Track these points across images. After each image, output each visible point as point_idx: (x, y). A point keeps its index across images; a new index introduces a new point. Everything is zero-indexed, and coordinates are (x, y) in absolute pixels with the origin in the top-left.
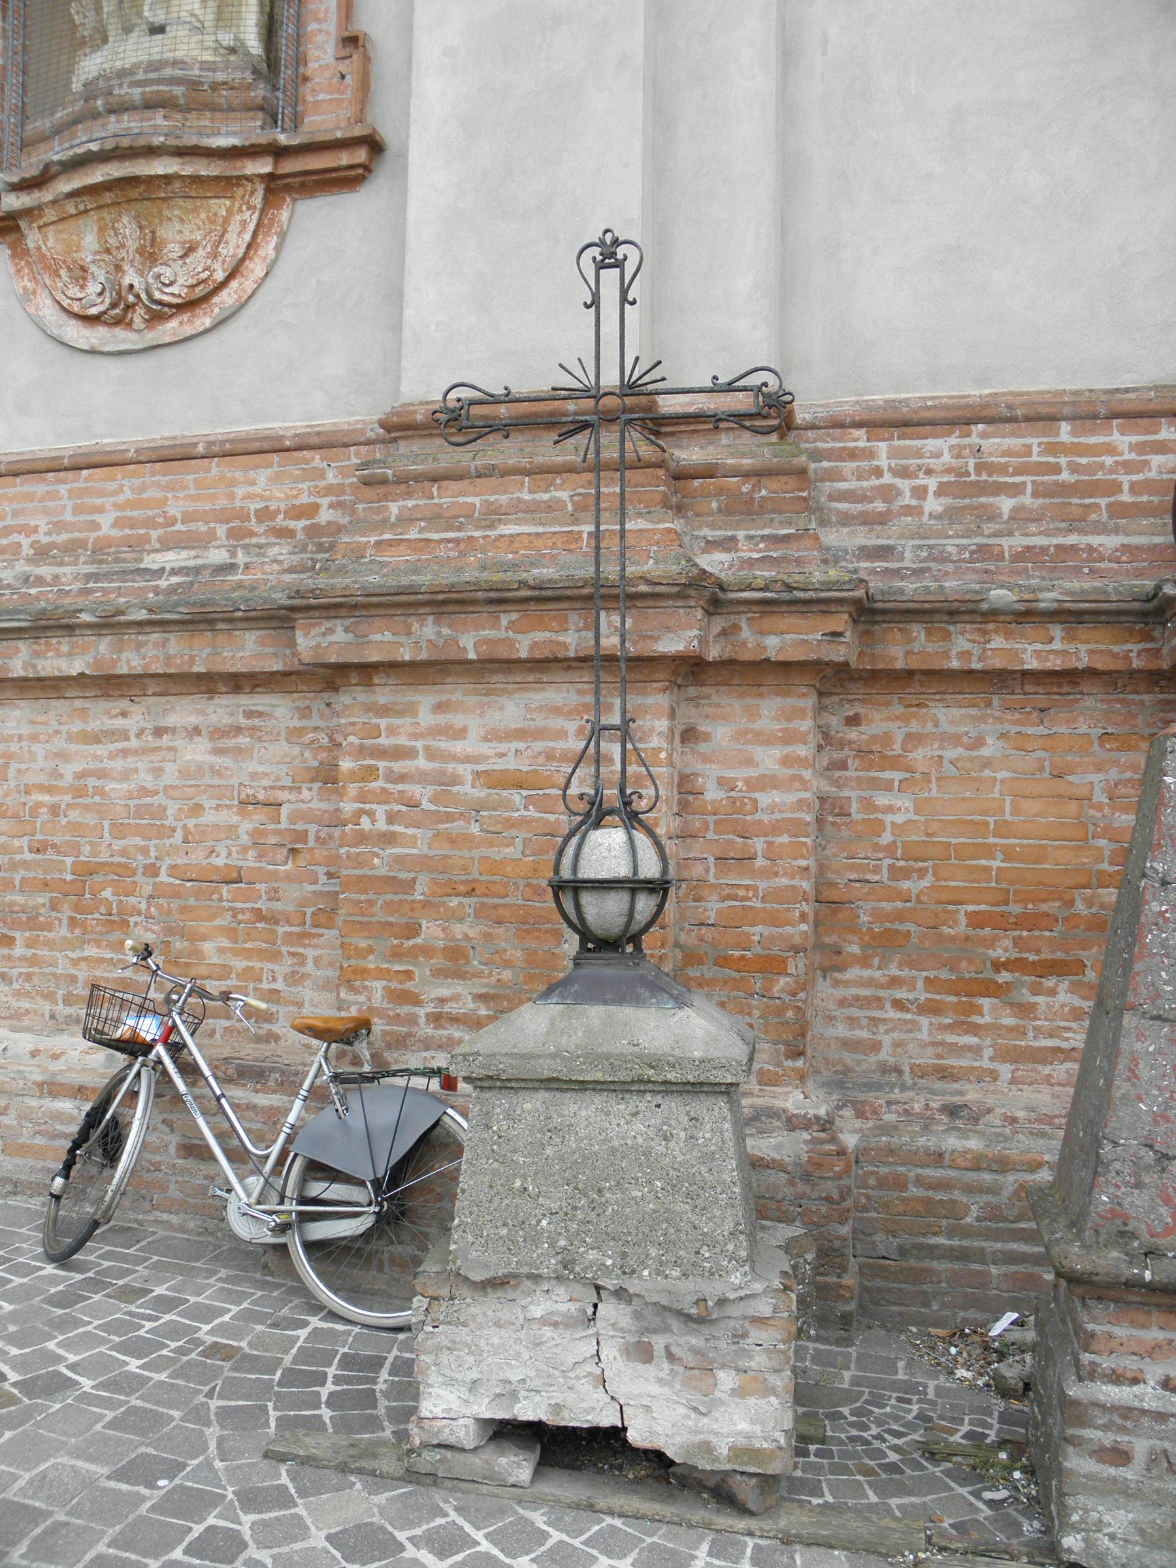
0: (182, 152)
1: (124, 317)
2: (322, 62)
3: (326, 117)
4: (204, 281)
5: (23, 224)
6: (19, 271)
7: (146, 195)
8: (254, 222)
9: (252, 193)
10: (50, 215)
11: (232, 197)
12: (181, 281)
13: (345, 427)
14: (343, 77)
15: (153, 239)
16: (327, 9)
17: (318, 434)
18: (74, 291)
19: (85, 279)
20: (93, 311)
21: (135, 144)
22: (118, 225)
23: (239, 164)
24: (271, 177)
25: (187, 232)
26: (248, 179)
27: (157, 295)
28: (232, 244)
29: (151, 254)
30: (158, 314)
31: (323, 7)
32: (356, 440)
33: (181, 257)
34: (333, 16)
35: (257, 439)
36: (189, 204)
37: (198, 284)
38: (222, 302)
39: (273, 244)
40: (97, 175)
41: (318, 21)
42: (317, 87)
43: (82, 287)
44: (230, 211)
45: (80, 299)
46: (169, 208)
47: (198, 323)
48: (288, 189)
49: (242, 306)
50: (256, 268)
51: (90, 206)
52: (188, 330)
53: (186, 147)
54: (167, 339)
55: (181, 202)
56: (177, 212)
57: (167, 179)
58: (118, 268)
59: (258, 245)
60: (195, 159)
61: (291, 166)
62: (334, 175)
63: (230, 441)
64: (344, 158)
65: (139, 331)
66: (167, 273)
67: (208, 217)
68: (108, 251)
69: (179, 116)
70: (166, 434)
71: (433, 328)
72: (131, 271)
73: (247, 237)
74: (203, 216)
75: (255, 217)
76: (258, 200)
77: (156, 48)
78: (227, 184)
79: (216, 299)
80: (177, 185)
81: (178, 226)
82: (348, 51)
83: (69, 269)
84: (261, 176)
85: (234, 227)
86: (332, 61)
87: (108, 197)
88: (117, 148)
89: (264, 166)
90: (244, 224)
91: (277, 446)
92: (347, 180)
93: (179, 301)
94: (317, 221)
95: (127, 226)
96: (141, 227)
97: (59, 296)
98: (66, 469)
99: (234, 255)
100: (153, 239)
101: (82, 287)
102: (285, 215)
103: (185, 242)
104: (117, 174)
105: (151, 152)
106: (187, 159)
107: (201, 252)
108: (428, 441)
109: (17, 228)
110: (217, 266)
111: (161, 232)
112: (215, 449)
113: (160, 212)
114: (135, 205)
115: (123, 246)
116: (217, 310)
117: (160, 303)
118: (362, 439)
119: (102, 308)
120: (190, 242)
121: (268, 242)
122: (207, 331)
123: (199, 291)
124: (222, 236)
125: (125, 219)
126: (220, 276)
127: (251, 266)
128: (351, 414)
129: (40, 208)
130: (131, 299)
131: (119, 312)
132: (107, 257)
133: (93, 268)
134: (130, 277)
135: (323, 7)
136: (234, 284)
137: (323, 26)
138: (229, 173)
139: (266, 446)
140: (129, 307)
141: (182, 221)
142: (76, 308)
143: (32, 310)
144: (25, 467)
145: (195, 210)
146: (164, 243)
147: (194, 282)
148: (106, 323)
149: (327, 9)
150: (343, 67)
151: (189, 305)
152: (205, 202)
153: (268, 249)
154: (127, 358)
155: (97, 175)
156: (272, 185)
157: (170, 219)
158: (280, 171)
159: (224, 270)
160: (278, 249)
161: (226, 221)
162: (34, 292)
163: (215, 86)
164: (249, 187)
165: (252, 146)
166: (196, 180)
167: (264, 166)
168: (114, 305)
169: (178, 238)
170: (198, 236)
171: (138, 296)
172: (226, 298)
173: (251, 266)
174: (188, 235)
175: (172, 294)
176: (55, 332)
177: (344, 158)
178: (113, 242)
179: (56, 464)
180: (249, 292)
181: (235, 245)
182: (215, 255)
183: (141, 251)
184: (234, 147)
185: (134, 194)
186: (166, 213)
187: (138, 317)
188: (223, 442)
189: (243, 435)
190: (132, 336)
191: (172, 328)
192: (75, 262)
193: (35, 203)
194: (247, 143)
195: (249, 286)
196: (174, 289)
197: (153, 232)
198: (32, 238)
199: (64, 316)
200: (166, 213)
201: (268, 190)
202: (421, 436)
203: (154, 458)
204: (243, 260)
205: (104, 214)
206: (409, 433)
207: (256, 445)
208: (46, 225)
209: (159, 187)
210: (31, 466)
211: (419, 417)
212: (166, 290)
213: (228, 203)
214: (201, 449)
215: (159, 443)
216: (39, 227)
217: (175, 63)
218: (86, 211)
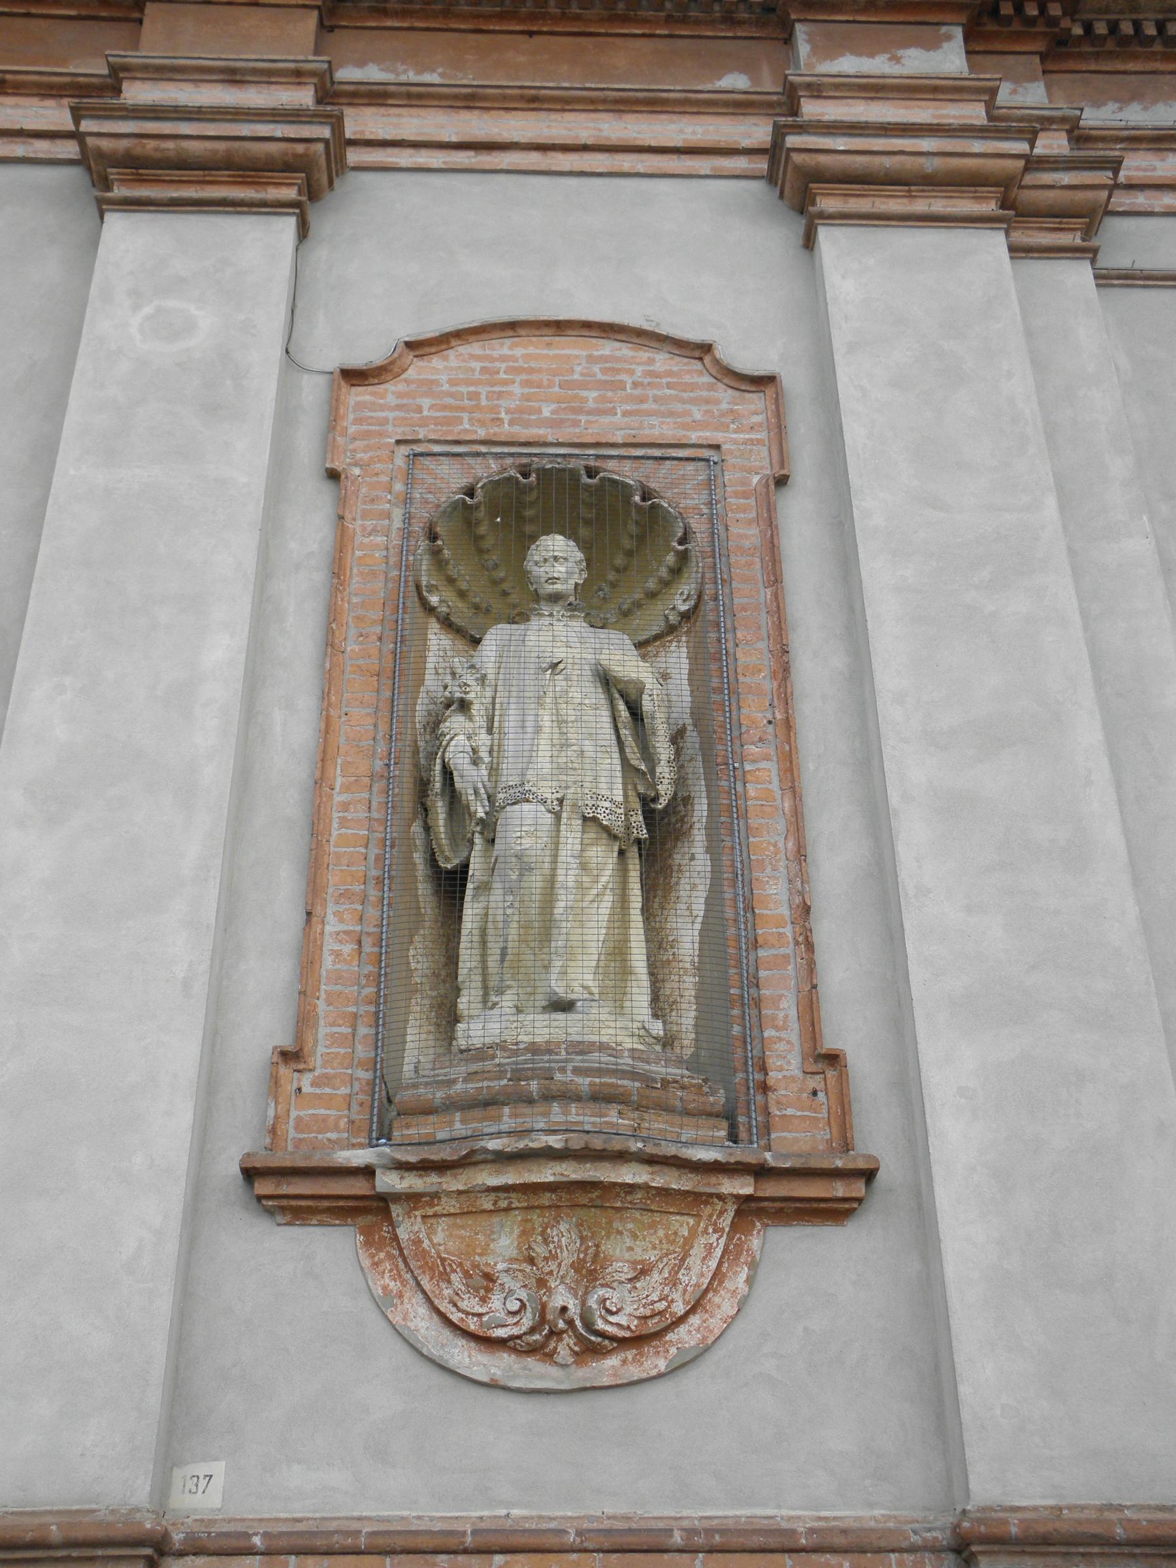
0: (651, 1161)
1: (544, 1345)
2: (788, 1074)
3: (797, 1136)
4: (660, 1313)
5: (396, 1210)
6: (376, 1264)
7: (599, 1202)
8: (722, 1246)
9: (721, 1213)
10: (449, 1205)
11: (698, 1216)
12: (629, 1309)
13: (872, 1524)
14: (815, 1093)
15: (596, 1255)
16: (786, 1016)
17: (844, 1532)
18: (471, 1303)
19: (488, 1290)
20: (501, 1333)
21: (608, 1147)
22: (552, 1232)
23: (713, 1180)
24: (749, 1198)
25: (639, 1250)
26: (721, 1197)
27: (600, 1325)
28: (695, 1270)
29: (589, 1272)
30: (593, 1346)
31: (781, 1015)
32: (896, 1545)
33: (630, 1280)
34: (794, 1025)
35: (755, 1532)
36: (646, 1218)
37: (652, 1317)
38: (680, 1341)
39: (743, 1276)
40: (547, 1174)
41: (777, 1028)
42: (784, 1100)
43: (484, 1300)
44: (693, 1233)
45: (480, 1315)
46: (621, 1219)
47: (648, 1364)
48: (761, 1213)
49: (707, 1349)
50: (723, 1304)
51: (516, 1204)
52: (635, 1372)
53: (665, 1157)
54: (606, 1381)
55: (637, 1215)
56: (630, 1226)
57: (631, 1188)
58: (542, 1283)
59: (724, 1275)
60: (666, 1169)
61: (772, 1189)
62: (823, 1205)
63: (723, 1532)
64: (839, 1189)
65: (564, 1366)
66: (614, 1297)
67: (666, 1236)
68: (531, 1261)
69: (636, 1114)
70: (609, 1511)
71: (998, 1412)
72: (561, 1288)
73: (713, 1264)
74: (661, 1233)
75: (723, 1241)
76: (726, 1222)
77: (543, 1028)
78: (695, 1200)
79: (670, 1337)
80: (639, 1195)
81: (629, 1242)
82: (819, 1067)
83: (467, 1274)
84: (737, 1197)
85: (697, 1251)
86: (798, 1073)
87: (546, 1199)
88: (586, 1148)
89: (744, 1187)
90: (709, 1248)
91: (788, 1543)
92: (835, 1212)
93: (627, 1334)
94: (785, 1247)
95: (565, 1235)
96: (582, 1238)
97: (445, 1307)
98: (466, 1551)
99: (697, 1285)
100: (596, 1255)
101: (484, 1300)
102: (755, 1243)
103: (634, 1263)
104: (574, 1177)
105: (622, 1157)
106: (657, 1168)
107: (656, 1276)
108: (1017, 1559)
109: (386, 1213)
110: (676, 1295)
111: (607, 1247)
112: (699, 1540)
113: (610, 1223)
114: (581, 1212)
115: (554, 1257)
116: (673, 1351)
117: (602, 1334)
118: (904, 1544)
119: (516, 1331)
120: (642, 1262)
121: (736, 1273)
122: (660, 1376)
123: (653, 1325)
124: (683, 1260)
125: (563, 1227)
126: (679, 1308)
127: (717, 1300)
128: (871, 1505)
129: (435, 1196)
130: (561, 1325)
131: (537, 1344)
132: (528, 1269)
133: (505, 1279)
134: (561, 1297)
135: (781, 1015)
136: (695, 1320)
137: (783, 1034)
138: (701, 1189)
139: (773, 1542)
140: (554, 1334)
141: (635, 1237)
142: (472, 1325)
143: (397, 1319)
144: (400, 1542)
145: (653, 1226)
146: (608, 1260)
147: (648, 1313)
148: (515, 1350)
149: (786, 1016)
150: (814, 1082)
151: (637, 1341)
152: (665, 1217)
153: (738, 1280)
154: (543, 1399)
155: (547, 1174)
156: (744, 1207)
157: (620, 1233)
158: (760, 1194)
159: (686, 1303)
160: (750, 1281)
161: (688, 1243)
162: (400, 1296)
163: (665, 1083)
164: (719, 1205)
165: (737, 1163)
166: (664, 1192)
167: (744, 1187)
168: (532, 1330)
169: (627, 1256)
170: (652, 1256)
171: (570, 1323)
172: (686, 1336)
173: (717, 1300)
174: (639, 1254)
175: (618, 1325)
176: (435, 1352)
177: (839, 1189)
178: (540, 1250)
179: (452, 1543)
180: (717, 1332)
181: (697, 1271)
182: (673, 1282)
183: (577, 1266)
184: (716, 1162)
185: (583, 1199)
186: (617, 1225)
187: (564, 1348)
188: (709, 1532)
189: (731, 1524)
190: (554, 1371)
191: (610, 1366)
192: (476, 1266)
193: (433, 1189)
194: (732, 1160)
195: (716, 1324)
196: (621, 1319)
197: (597, 1246)
198: (408, 1228)
199: (447, 1333)
200: (617, 1225)
201: (738, 1213)
202: (1010, 1553)
203: (606, 1546)
204: (706, 1291)
205: (534, 1216)
206: (996, 1548)
207: (758, 1541)
208: (435, 1215)
209: (618, 1195)
210: (410, 1543)
211: (1014, 1530)
212: (612, 1319)
213: (691, 1221)
214: (678, 1539)
215: (607, 1525)
216: (424, 1217)
217: (602, 1047)
218: (508, 1209)
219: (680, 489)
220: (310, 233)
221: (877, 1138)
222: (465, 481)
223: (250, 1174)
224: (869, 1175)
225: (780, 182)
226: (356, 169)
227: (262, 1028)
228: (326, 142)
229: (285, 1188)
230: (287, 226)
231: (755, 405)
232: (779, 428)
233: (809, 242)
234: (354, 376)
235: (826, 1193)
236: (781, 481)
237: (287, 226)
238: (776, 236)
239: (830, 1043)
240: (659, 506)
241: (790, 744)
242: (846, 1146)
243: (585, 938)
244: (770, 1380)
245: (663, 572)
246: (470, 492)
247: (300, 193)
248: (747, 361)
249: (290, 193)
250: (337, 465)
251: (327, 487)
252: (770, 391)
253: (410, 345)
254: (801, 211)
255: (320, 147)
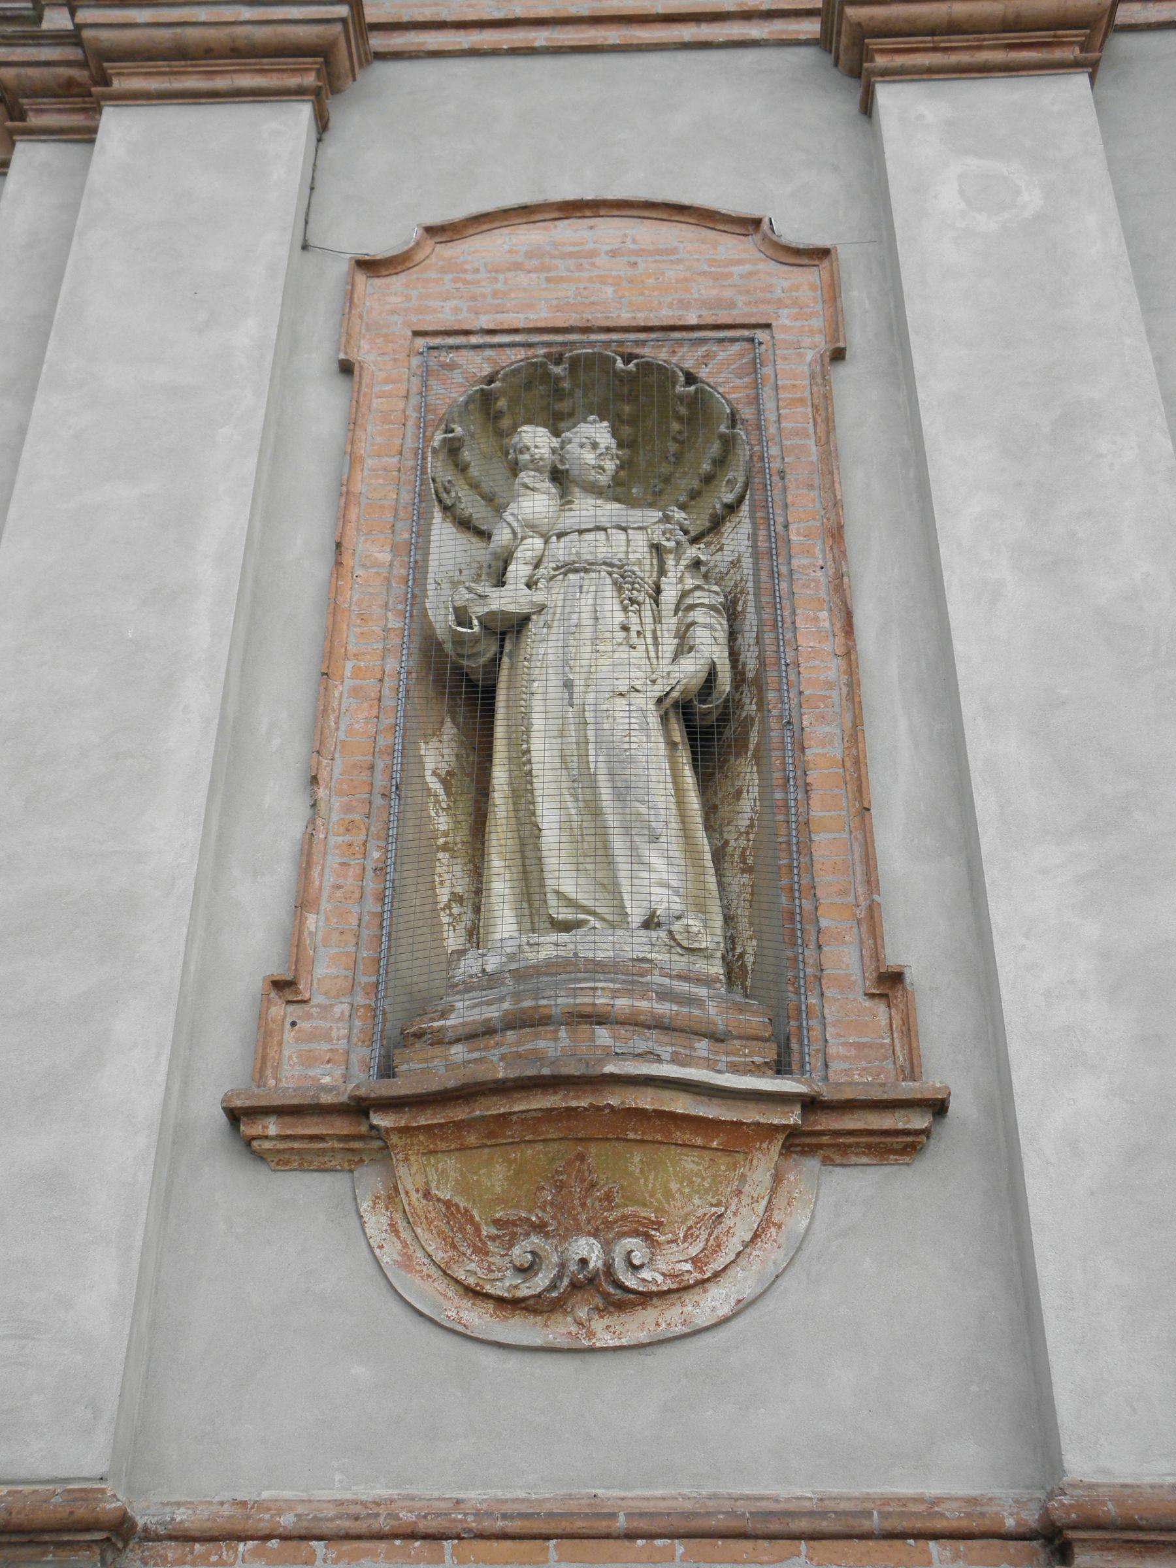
3: (848, 1049)
94: (837, 1200)
219: (720, 371)
220: (330, 125)
221: (946, 1068)
222: (487, 370)
223: (235, 1116)
224: (939, 1107)
225: (910, 1139)
226: (381, 56)
227: (254, 951)
228: (343, 20)
229: (266, 1127)
230: (304, 111)
231: (807, 279)
232: (833, 294)
233: (867, 107)
234: (369, 266)
235: (887, 1127)
236: (838, 355)
237: (304, 111)
238: (830, 105)
239: (893, 958)
240: (703, 390)
241: (857, 748)
242: (912, 1071)
243: (559, 740)
244: (815, 1341)
245: (706, 467)
246: (490, 380)
247: (319, 77)
248: (794, 229)
249: (310, 80)
250: (353, 357)
251: (340, 382)
252: (825, 264)
253: (431, 231)
254: (856, 72)
255: (338, 28)
